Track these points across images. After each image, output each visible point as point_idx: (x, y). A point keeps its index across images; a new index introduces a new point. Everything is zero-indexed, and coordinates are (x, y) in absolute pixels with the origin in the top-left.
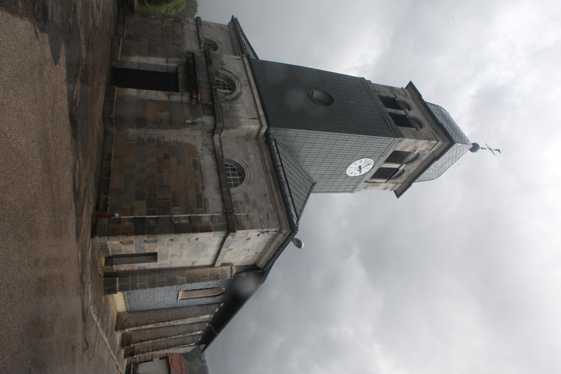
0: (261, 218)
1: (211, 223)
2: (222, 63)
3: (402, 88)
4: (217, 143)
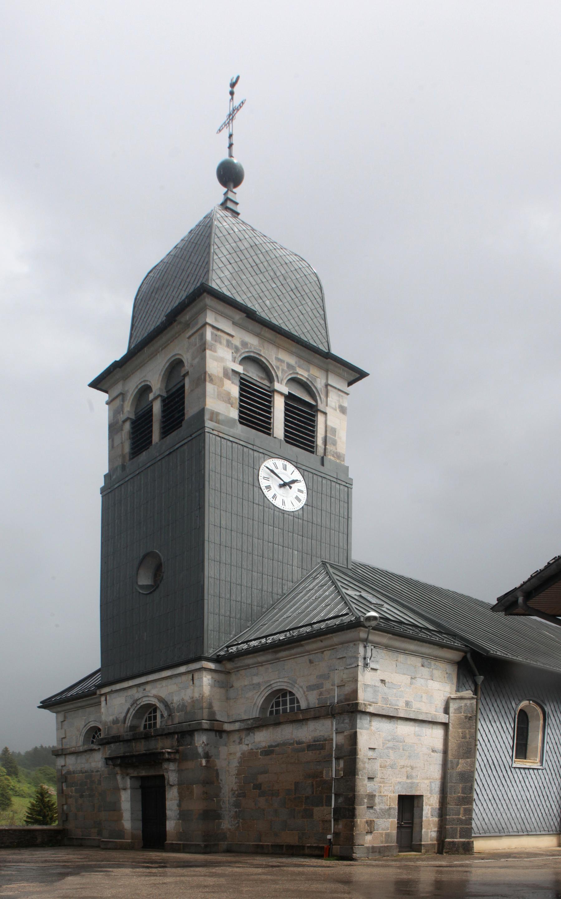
0: (343, 668)
1: (346, 734)
2: (115, 722)
3: (108, 403)
4: (237, 726)
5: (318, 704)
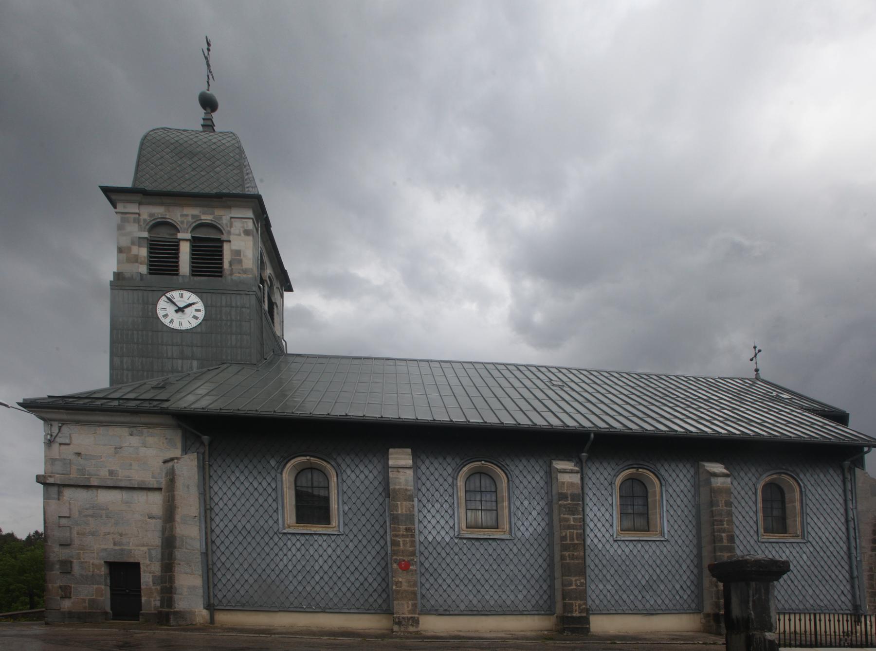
5: (394, 490)
